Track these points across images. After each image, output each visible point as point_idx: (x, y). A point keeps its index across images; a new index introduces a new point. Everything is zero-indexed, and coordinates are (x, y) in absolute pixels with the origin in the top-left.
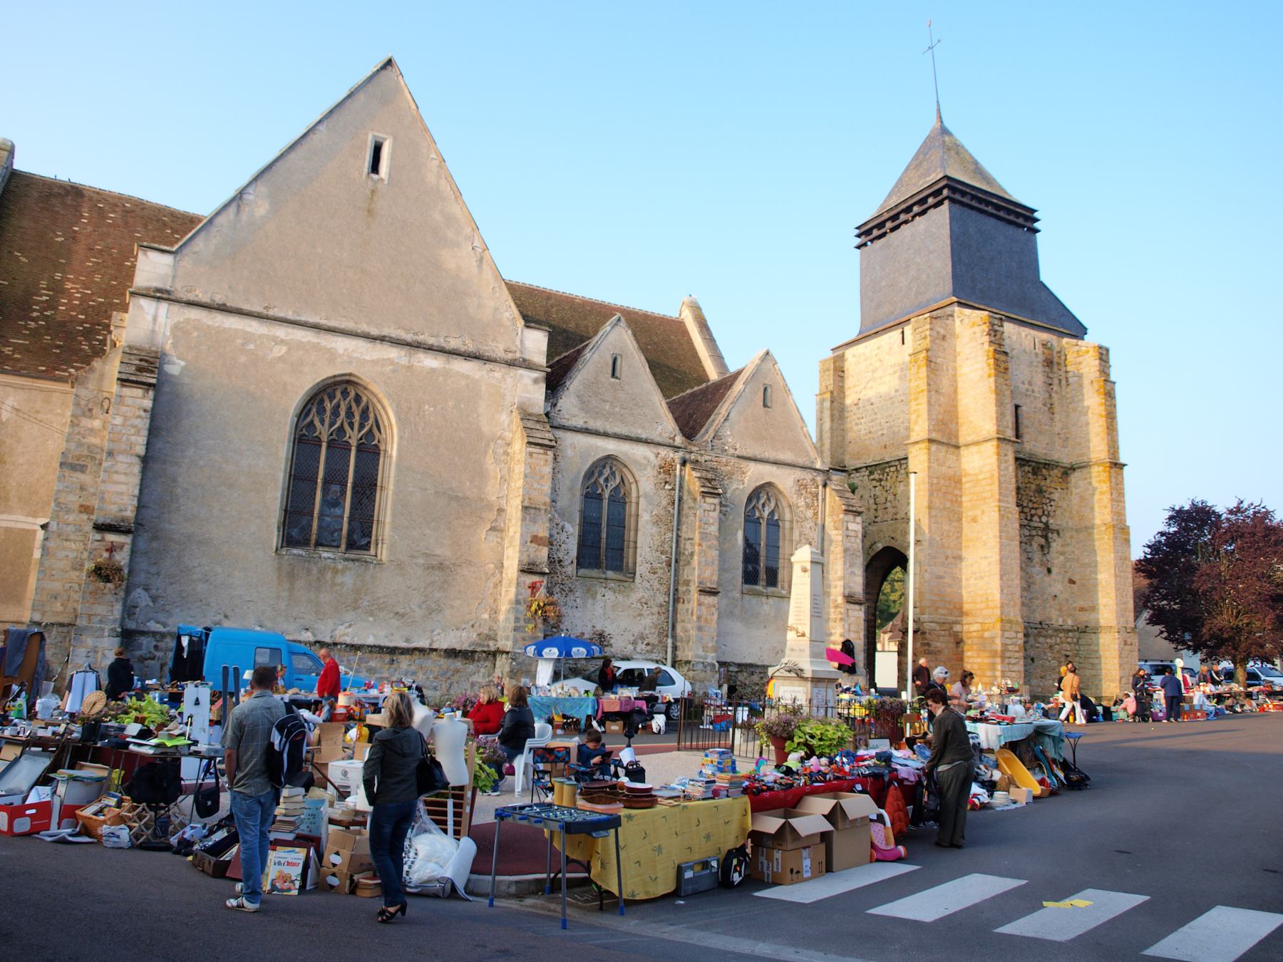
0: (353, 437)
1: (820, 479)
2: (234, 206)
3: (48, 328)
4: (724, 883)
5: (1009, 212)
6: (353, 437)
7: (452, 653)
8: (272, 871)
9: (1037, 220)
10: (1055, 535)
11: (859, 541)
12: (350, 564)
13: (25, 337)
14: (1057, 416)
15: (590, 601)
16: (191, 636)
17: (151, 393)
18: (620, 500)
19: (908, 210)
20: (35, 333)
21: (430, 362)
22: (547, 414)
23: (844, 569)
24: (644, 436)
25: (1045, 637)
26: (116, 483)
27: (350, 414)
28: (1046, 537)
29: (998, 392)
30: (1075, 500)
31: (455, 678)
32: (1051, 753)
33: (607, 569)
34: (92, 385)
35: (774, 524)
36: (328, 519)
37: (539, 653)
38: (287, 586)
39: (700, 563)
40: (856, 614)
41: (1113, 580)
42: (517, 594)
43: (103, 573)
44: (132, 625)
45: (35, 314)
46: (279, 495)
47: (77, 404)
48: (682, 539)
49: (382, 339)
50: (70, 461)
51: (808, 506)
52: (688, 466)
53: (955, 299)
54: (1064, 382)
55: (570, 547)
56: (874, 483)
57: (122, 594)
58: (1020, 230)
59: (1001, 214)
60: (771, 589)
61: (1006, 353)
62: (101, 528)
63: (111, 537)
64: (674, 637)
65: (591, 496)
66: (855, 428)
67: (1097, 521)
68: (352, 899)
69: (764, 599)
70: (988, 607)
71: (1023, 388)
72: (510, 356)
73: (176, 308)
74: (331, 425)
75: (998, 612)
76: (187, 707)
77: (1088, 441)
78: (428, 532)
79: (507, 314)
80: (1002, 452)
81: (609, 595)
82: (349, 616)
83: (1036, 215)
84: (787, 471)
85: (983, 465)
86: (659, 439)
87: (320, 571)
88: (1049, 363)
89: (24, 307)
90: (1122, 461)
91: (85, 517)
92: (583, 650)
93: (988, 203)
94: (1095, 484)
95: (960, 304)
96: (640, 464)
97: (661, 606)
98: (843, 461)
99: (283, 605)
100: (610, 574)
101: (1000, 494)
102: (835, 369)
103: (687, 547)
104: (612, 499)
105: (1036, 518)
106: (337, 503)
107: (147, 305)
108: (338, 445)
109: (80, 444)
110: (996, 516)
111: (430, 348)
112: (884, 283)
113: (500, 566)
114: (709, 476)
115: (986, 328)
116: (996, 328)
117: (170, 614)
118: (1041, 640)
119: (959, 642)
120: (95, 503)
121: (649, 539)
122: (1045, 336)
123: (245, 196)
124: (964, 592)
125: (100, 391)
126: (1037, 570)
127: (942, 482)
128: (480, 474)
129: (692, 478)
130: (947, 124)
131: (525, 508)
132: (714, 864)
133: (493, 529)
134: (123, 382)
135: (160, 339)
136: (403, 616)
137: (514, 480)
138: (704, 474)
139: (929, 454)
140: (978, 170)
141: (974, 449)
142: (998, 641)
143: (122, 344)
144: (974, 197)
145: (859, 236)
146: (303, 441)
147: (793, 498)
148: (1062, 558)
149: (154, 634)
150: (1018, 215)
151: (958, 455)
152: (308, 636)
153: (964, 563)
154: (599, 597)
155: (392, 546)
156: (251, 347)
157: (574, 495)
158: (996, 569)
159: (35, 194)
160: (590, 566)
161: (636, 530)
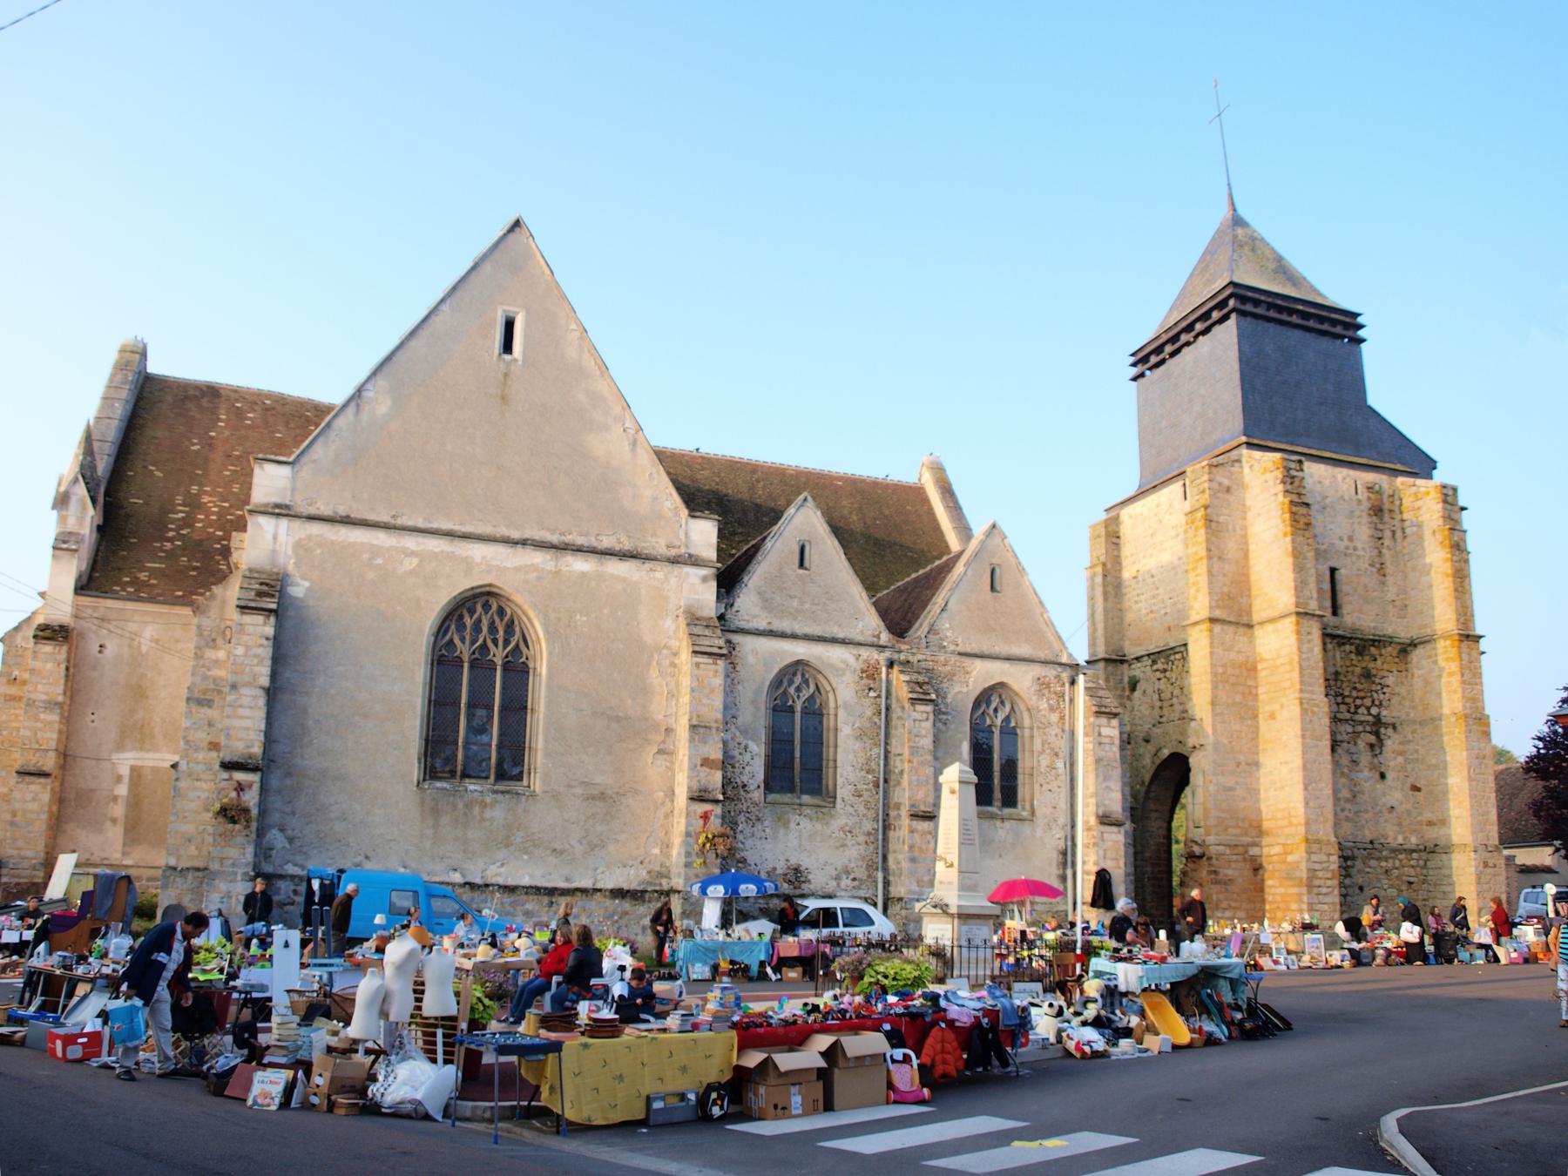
0: (498, 655)
1: (1065, 676)
2: (353, 404)
3: (184, 549)
4: (701, 1116)
5: (1322, 320)
6: (498, 655)
7: (619, 893)
8: (256, 1089)
9: (1361, 327)
10: (1390, 731)
11: (1116, 749)
12: (500, 797)
13: (160, 560)
14: (1390, 580)
15: (782, 831)
16: (322, 879)
17: (272, 619)
18: (815, 712)
19: (1189, 328)
20: (172, 556)
21: (580, 565)
22: (721, 618)
23: (1097, 783)
24: (841, 635)
25: (1379, 859)
26: (242, 717)
27: (493, 629)
28: (1377, 734)
29: (1297, 554)
30: (1418, 683)
31: (624, 921)
32: (1228, 998)
33: (802, 792)
34: (213, 614)
35: (1010, 732)
36: (474, 748)
37: (703, 891)
38: (431, 822)
39: (910, 783)
40: (1114, 837)
41: (1466, 784)
42: (688, 825)
43: (230, 814)
44: (268, 869)
45: (171, 534)
46: (418, 723)
47: (200, 635)
48: (891, 756)
49: (524, 543)
50: (197, 695)
51: (1052, 709)
52: (896, 668)
53: (1244, 439)
54: (1399, 534)
55: (754, 769)
56: (1158, 675)
57: (254, 836)
58: (1338, 342)
59: (1311, 323)
60: (1007, 811)
61: (1307, 505)
62: (228, 766)
63: (240, 776)
64: (885, 870)
65: (780, 709)
66: (1135, 607)
67: (1446, 711)
68: (329, 1118)
69: (998, 823)
70: (1291, 824)
71: (1341, 545)
72: (673, 552)
73: (296, 524)
74: (473, 643)
75: (1302, 830)
76: (275, 949)
77: (1432, 608)
78: (585, 757)
79: (668, 504)
80: (1303, 631)
81: (806, 824)
82: (501, 854)
83: (1360, 320)
84: (1023, 667)
85: (1282, 649)
86: (860, 638)
87: (466, 806)
88: (1377, 511)
89: (160, 525)
90: (1478, 632)
91: (214, 754)
92: (753, 887)
93: (1291, 312)
94: (1441, 663)
95: (1249, 445)
96: (837, 669)
97: (869, 834)
98: (1122, 648)
99: (428, 844)
100: (806, 798)
101: (1302, 682)
102: (1108, 535)
103: (897, 764)
104: (806, 711)
105: (1362, 710)
106: (484, 729)
107: (265, 522)
108: (481, 665)
109: (205, 678)
110: (1296, 710)
111: (579, 550)
112: (1164, 424)
113: (671, 793)
114: (921, 679)
115: (1279, 474)
116: (1293, 473)
117: (307, 856)
118: (1373, 863)
119: (1257, 868)
120: (223, 740)
121: (851, 756)
122: (1371, 477)
123: (365, 394)
124: (1263, 807)
125: (223, 619)
126: (1365, 776)
127: (1230, 671)
128: (644, 691)
129: (899, 679)
130: (1243, 212)
131: (693, 727)
132: (692, 1097)
133: (660, 752)
134: (243, 609)
135: (281, 560)
136: (561, 852)
137: (681, 690)
138: (915, 677)
139: (1212, 637)
140: (1282, 269)
141: (1269, 628)
142: (1303, 866)
143: (243, 567)
144: (1270, 306)
145: (1134, 365)
146: (443, 662)
147: (1033, 700)
148: (1400, 759)
149: (293, 877)
150: (1334, 322)
151: (1252, 638)
152: (457, 878)
153: (1262, 771)
154: (792, 825)
155: (546, 776)
156: (379, 561)
157: (758, 710)
158: (1298, 776)
159: (170, 399)
160: (782, 790)
161: (836, 746)
